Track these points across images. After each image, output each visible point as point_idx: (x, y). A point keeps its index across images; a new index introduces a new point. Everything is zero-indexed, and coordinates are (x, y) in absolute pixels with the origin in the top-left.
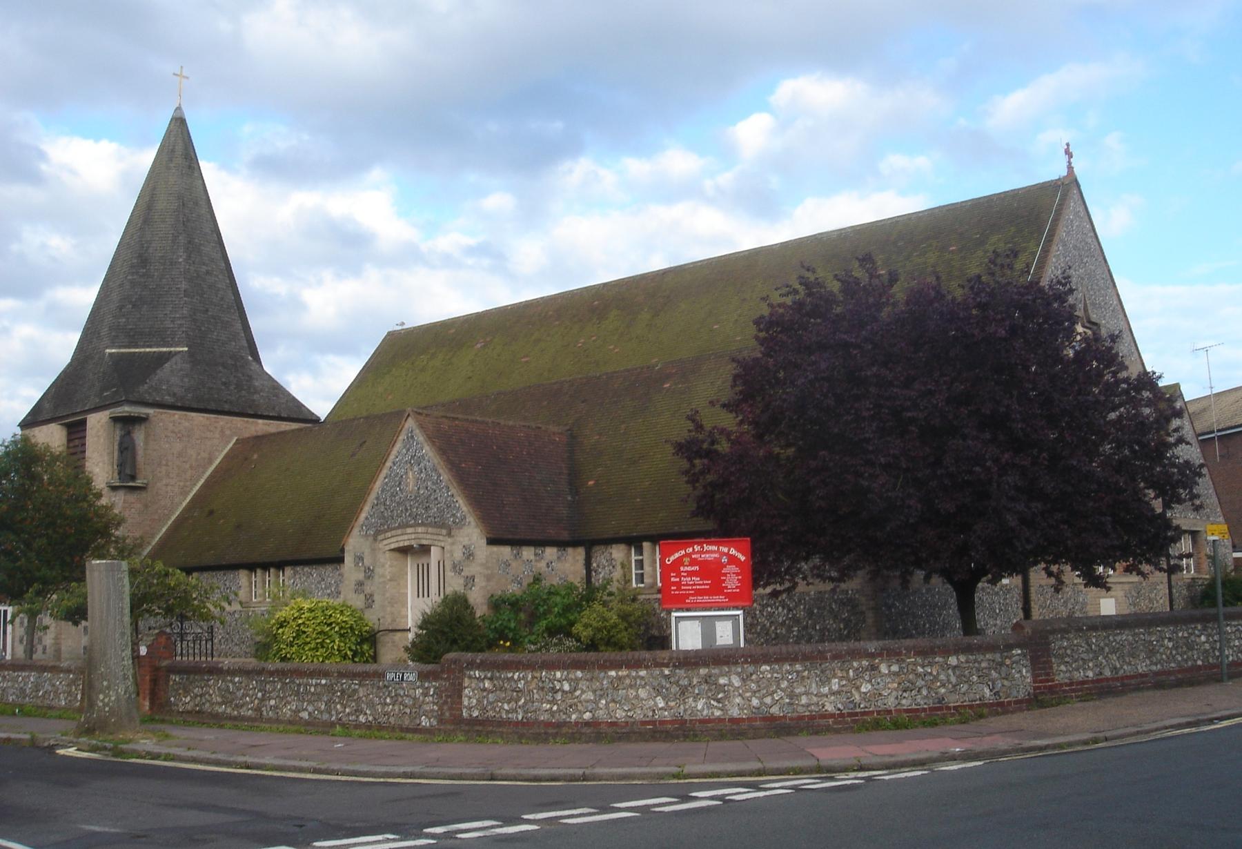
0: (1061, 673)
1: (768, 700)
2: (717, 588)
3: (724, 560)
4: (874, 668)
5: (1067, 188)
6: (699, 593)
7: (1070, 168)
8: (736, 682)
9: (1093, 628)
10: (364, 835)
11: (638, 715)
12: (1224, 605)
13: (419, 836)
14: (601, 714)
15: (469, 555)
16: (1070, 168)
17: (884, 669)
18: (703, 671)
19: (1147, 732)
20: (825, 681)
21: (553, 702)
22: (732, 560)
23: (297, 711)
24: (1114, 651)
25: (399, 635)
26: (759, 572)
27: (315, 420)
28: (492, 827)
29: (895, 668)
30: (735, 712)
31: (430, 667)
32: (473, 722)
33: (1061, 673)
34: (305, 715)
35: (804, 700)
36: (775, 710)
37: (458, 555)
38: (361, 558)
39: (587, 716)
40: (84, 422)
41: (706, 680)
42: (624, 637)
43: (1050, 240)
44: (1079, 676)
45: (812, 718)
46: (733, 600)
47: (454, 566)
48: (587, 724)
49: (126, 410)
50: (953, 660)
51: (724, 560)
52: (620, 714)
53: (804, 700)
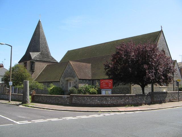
0: (155, 99)
1: (114, 102)
2: (108, 86)
3: (109, 82)
4: (128, 98)
5: (161, 32)
6: (106, 87)
7: (162, 29)
8: (109, 99)
9: (160, 93)
10: (23, 121)
11: (96, 103)
12: (131, 94)
13: (61, 119)
14: (91, 103)
15: (76, 81)
16: (162, 29)
17: (130, 98)
18: (105, 98)
19: (166, 108)
20: (121, 100)
21: (84, 101)
22: (110, 82)
23: (51, 101)
24: (163, 97)
25: (67, 92)
26: (114, 84)
27: (57, 63)
28: (27, 122)
29: (131, 98)
30: (109, 103)
31: (68, 96)
32: (74, 104)
33: (155, 99)
34: (52, 102)
35: (119, 102)
36: (115, 103)
37: (75, 81)
38: (62, 81)
39: (89, 103)
40: (27, 62)
41: (105, 99)
42: (97, 93)
43: (158, 39)
44: (158, 100)
45: (119, 104)
46: (110, 88)
47: (74, 83)
48: (89, 104)
49: (25, 62)
50: (140, 97)
51: (109, 82)
52: (93, 103)
53: (119, 102)
